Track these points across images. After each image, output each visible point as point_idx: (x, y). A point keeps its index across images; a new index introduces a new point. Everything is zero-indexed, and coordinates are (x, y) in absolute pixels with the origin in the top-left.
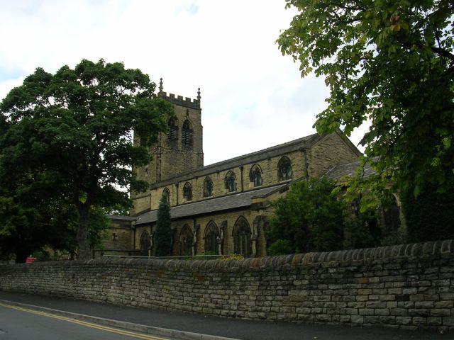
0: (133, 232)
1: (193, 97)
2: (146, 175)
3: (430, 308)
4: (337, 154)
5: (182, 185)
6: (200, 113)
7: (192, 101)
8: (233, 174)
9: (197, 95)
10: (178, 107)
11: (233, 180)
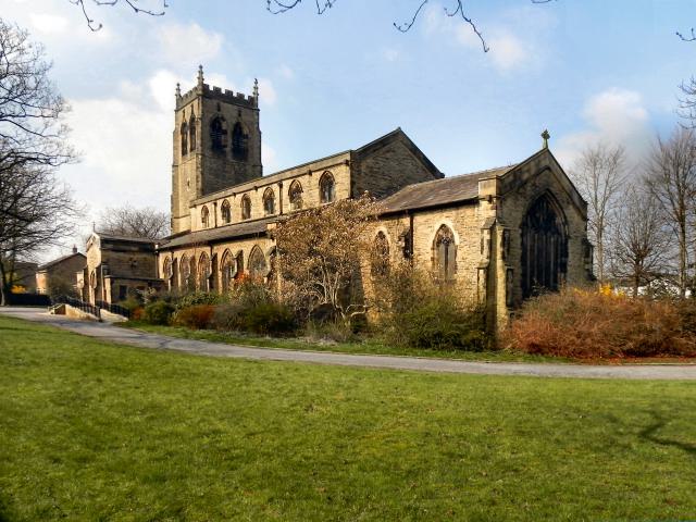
1: (247, 93)
5: (220, 202)
7: (246, 98)
8: (272, 193)
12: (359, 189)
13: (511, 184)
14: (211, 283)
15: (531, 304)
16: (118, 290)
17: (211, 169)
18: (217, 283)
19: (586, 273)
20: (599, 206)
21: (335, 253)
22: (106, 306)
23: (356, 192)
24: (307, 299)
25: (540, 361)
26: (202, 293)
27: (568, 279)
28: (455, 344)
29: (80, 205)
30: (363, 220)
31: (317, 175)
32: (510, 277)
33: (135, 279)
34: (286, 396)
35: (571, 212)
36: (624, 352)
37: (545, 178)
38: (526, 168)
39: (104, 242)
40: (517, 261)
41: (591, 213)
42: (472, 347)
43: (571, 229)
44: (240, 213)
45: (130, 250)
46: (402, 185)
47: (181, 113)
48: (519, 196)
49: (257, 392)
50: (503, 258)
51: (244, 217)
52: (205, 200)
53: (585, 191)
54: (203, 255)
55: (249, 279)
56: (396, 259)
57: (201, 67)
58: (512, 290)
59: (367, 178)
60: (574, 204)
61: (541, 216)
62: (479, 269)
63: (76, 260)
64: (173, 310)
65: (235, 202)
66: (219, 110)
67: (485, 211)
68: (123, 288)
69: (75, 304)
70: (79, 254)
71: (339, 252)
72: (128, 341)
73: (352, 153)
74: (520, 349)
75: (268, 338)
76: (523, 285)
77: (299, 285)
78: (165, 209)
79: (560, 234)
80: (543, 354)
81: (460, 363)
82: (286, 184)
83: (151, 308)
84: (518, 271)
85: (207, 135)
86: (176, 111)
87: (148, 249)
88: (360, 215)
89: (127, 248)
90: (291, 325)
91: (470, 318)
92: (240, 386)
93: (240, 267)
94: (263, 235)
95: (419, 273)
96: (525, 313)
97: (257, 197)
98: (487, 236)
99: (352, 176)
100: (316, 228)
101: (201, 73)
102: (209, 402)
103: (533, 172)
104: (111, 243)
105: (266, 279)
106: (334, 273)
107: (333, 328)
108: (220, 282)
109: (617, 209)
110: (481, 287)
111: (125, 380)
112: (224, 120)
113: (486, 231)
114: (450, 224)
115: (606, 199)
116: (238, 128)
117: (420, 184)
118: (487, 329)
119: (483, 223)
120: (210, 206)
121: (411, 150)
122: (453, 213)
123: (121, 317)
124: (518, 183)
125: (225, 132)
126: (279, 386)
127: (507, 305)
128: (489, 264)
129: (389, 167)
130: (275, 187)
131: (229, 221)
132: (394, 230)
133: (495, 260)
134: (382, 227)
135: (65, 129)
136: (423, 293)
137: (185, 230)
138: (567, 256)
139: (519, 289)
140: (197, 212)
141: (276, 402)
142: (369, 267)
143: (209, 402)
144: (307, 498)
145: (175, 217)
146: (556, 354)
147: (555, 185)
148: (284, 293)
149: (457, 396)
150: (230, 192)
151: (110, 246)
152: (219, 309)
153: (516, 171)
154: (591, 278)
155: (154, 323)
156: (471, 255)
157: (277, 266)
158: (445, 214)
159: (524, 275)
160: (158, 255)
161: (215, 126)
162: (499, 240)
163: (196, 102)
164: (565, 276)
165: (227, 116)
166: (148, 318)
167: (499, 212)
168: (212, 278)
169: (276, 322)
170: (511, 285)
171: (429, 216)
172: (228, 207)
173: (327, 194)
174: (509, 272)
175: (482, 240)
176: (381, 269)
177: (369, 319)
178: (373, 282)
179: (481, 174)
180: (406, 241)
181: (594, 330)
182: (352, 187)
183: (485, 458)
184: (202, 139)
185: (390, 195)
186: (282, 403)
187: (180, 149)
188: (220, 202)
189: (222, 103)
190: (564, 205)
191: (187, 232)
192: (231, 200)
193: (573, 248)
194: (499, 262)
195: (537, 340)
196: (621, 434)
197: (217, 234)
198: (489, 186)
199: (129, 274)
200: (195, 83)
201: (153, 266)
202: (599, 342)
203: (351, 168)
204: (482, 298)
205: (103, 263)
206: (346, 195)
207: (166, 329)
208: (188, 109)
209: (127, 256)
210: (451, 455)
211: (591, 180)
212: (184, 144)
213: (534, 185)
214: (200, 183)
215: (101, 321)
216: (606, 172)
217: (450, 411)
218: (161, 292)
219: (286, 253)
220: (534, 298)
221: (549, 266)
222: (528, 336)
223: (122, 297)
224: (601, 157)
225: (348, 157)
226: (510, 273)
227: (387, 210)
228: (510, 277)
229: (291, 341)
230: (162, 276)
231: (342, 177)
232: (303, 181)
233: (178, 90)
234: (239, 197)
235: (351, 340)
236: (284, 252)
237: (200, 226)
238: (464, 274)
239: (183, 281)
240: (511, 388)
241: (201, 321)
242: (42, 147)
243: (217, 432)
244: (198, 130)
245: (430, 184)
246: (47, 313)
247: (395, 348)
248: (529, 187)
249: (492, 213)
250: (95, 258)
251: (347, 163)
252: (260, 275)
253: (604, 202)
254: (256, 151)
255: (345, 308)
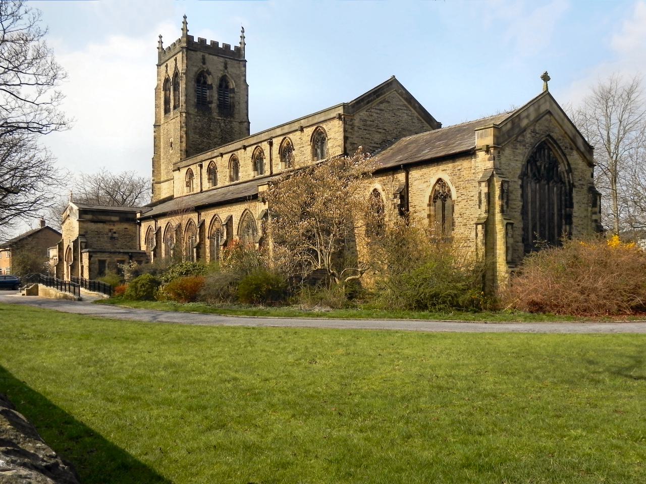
0: (138, 226)
1: (234, 43)
2: (171, 152)
3: (146, 325)
4: (397, 123)
5: (205, 165)
6: (245, 66)
7: (232, 48)
8: (262, 152)
9: (240, 40)
10: (211, 56)
11: (262, 159)
12: (352, 144)
13: (508, 131)
14: (198, 253)
15: (531, 259)
16: (96, 266)
17: (196, 128)
18: (205, 253)
19: (594, 224)
20: (612, 148)
21: (329, 214)
22: (83, 284)
23: (349, 147)
24: (300, 265)
25: (542, 320)
26: (190, 263)
27: (574, 232)
28: (452, 305)
29: (61, 174)
30: (357, 178)
31: (309, 131)
32: (510, 231)
33: (114, 253)
34: (290, 353)
35: (575, 158)
36: (632, 308)
37: (546, 124)
38: (525, 114)
39: (82, 212)
40: (518, 215)
41: (597, 156)
42: (471, 307)
43: (576, 177)
44: (228, 174)
45: (108, 219)
46: (397, 138)
47: (163, 67)
48: (518, 145)
49: (262, 351)
50: (502, 211)
51: (232, 179)
52: (189, 162)
53: (593, 134)
54: (190, 223)
55: (240, 246)
56: (391, 218)
57: (185, 17)
58: (512, 245)
59: (360, 132)
60: (578, 149)
61: (542, 164)
62: (477, 224)
63: (46, 236)
64: (159, 283)
65: (222, 164)
66: (204, 63)
67: (483, 163)
68: (102, 263)
69: (50, 283)
70: (48, 227)
71: (333, 213)
72: (119, 316)
73: (345, 106)
74: (520, 309)
75: (261, 307)
76: (525, 240)
77: (292, 250)
78: (144, 173)
79: (563, 183)
80: (544, 313)
81: (456, 324)
82: (277, 142)
83: (136, 283)
84: (519, 225)
85: (192, 91)
86: (159, 66)
87: (130, 218)
88: (353, 172)
89: (108, 218)
90: (285, 293)
91: (468, 277)
92: (245, 347)
93: (229, 233)
94: (255, 197)
95: (415, 231)
96: (526, 270)
97: (245, 158)
98: (484, 189)
99: (345, 131)
100: (310, 190)
101: (185, 23)
102: (221, 360)
103: (532, 117)
104: (91, 214)
105: (257, 245)
106: (329, 235)
107: (327, 294)
108: (208, 250)
109: (632, 151)
110: (480, 244)
111: (135, 346)
112: (209, 73)
113: (483, 184)
114: (446, 178)
115: (619, 140)
116: (223, 83)
117: (416, 136)
118: (487, 290)
119: (481, 175)
120: (195, 169)
121: (406, 99)
122: (449, 166)
123: (101, 294)
124: (517, 131)
125: (210, 87)
126: (282, 345)
127: (508, 263)
128: (488, 219)
129: (384, 118)
130: (265, 146)
131: (215, 184)
132: (388, 187)
133: (494, 215)
134: (377, 184)
135: (59, 95)
136: (419, 252)
137: (167, 195)
138: (571, 206)
139: (521, 244)
140: (181, 175)
141: (281, 358)
142: (364, 228)
143: (221, 360)
144: (322, 413)
145: (157, 182)
146: (559, 312)
147: (557, 130)
148: (277, 259)
149: (450, 349)
150: (216, 152)
151: (89, 217)
152: (210, 279)
153: (515, 118)
154: (600, 229)
155: (139, 298)
156: (468, 209)
157: (269, 231)
158: (442, 167)
159: (525, 229)
160: (140, 225)
161: (200, 80)
162: (497, 192)
163: (179, 56)
164: (571, 228)
165: (212, 70)
166: (133, 293)
167: (497, 163)
168: (200, 247)
169: (269, 290)
170: (511, 241)
171: (425, 170)
172: (215, 168)
173: (319, 151)
174: (509, 226)
175: (480, 193)
176: (376, 229)
177: (364, 285)
178: (368, 244)
179: (478, 123)
180: (402, 198)
181: (600, 284)
182: (345, 142)
183: (469, 389)
184: (186, 95)
185: (384, 149)
186: (287, 358)
187: (163, 107)
188: (205, 165)
189: (207, 56)
190: (566, 151)
191: (171, 198)
192: (218, 161)
193: (579, 198)
194: (498, 217)
195: (537, 298)
196: (600, 373)
197: (203, 199)
198: (486, 136)
199: (108, 246)
200: (179, 35)
201: (135, 237)
202: (605, 298)
203: (345, 123)
204: (480, 255)
205: (81, 235)
206: (339, 151)
207: (154, 304)
208: (171, 63)
209: (107, 227)
210: (440, 388)
211: (603, 119)
212: (167, 102)
213: (534, 131)
214: (184, 145)
215: (80, 299)
216: (620, 110)
217: (443, 360)
218: (143, 264)
219: (278, 216)
220: (534, 253)
221: (553, 218)
222: (528, 294)
223: (101, 273)
224: (613, 93)
225: (341, 111)
226: (509, 227)
227: (382, 166)
228: (510, 231)
229: (285, 309)
230: (144, 248)
231: (335, 132)
232: (295, 138)
233: (161, 42)
234: (227, 157)
235: (346, 306)
236: (276, 215)
237: (186, 191)
238: (461, 231)
239: (167, 253)
240: (504, 341)
241: (190, 294)
242: (32, 115)
243: (235, 379)
244: (182, 86)
245: (426, 135)
246: (19, 295)
247: (391, 311)
248: (528, 135)
249: (490, 164)
250: (71, 230)
251: (339, 117)
252: (251, 242)
253: (618, 142)
254: (243, 105)
255: (339, 272)
